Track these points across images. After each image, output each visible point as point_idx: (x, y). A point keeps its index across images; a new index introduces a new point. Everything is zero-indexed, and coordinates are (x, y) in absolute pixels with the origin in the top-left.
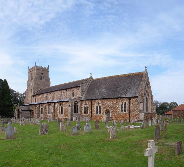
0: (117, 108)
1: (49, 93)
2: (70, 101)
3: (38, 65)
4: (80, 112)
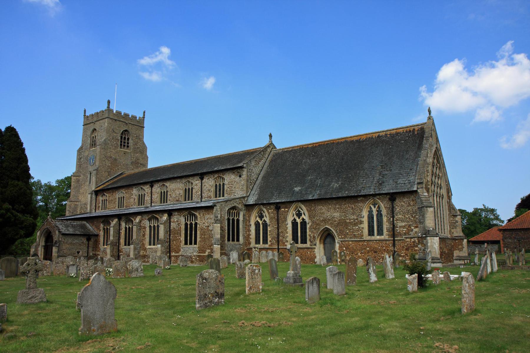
0: (355, 225)
1: (148, 186)
2: (218, 207)
3: (115, 108)
4: (244, 237)
